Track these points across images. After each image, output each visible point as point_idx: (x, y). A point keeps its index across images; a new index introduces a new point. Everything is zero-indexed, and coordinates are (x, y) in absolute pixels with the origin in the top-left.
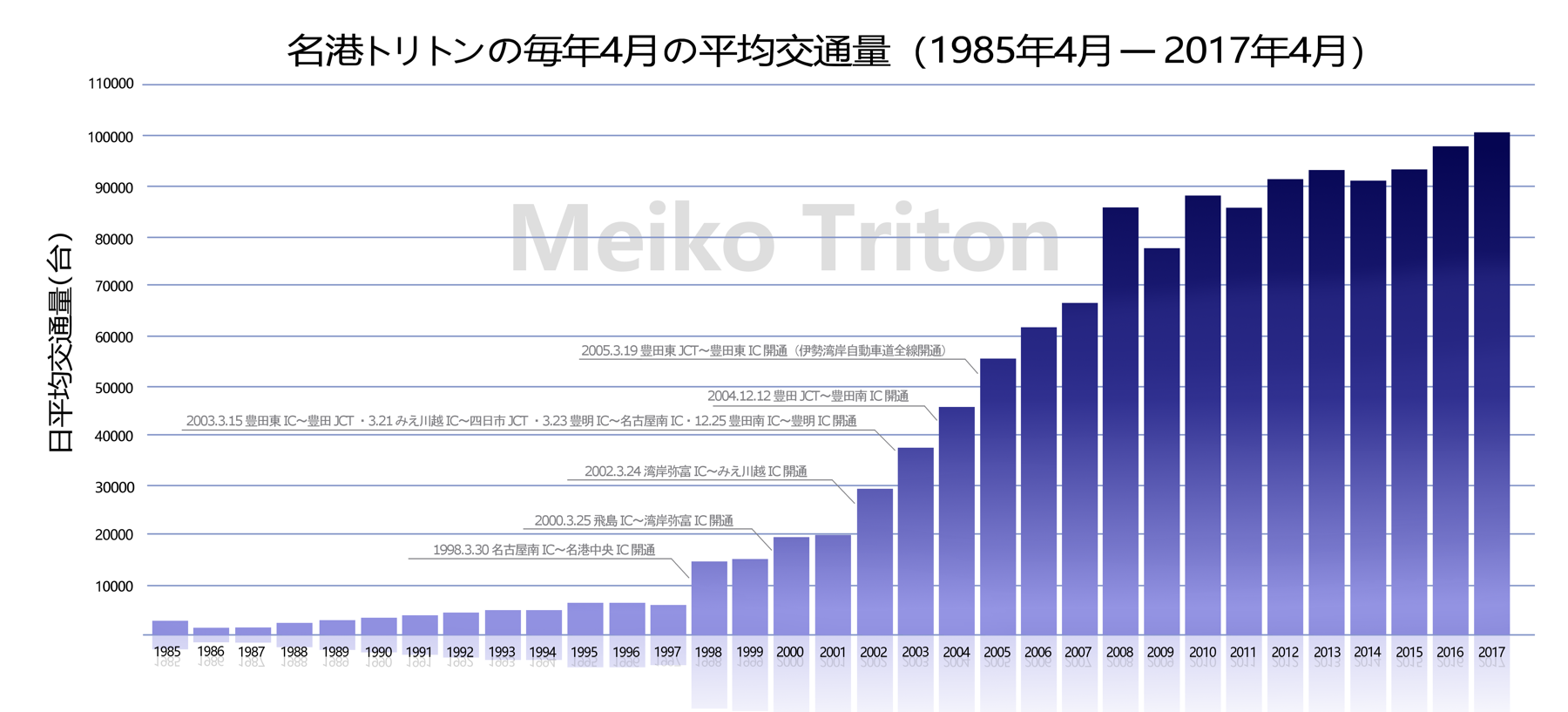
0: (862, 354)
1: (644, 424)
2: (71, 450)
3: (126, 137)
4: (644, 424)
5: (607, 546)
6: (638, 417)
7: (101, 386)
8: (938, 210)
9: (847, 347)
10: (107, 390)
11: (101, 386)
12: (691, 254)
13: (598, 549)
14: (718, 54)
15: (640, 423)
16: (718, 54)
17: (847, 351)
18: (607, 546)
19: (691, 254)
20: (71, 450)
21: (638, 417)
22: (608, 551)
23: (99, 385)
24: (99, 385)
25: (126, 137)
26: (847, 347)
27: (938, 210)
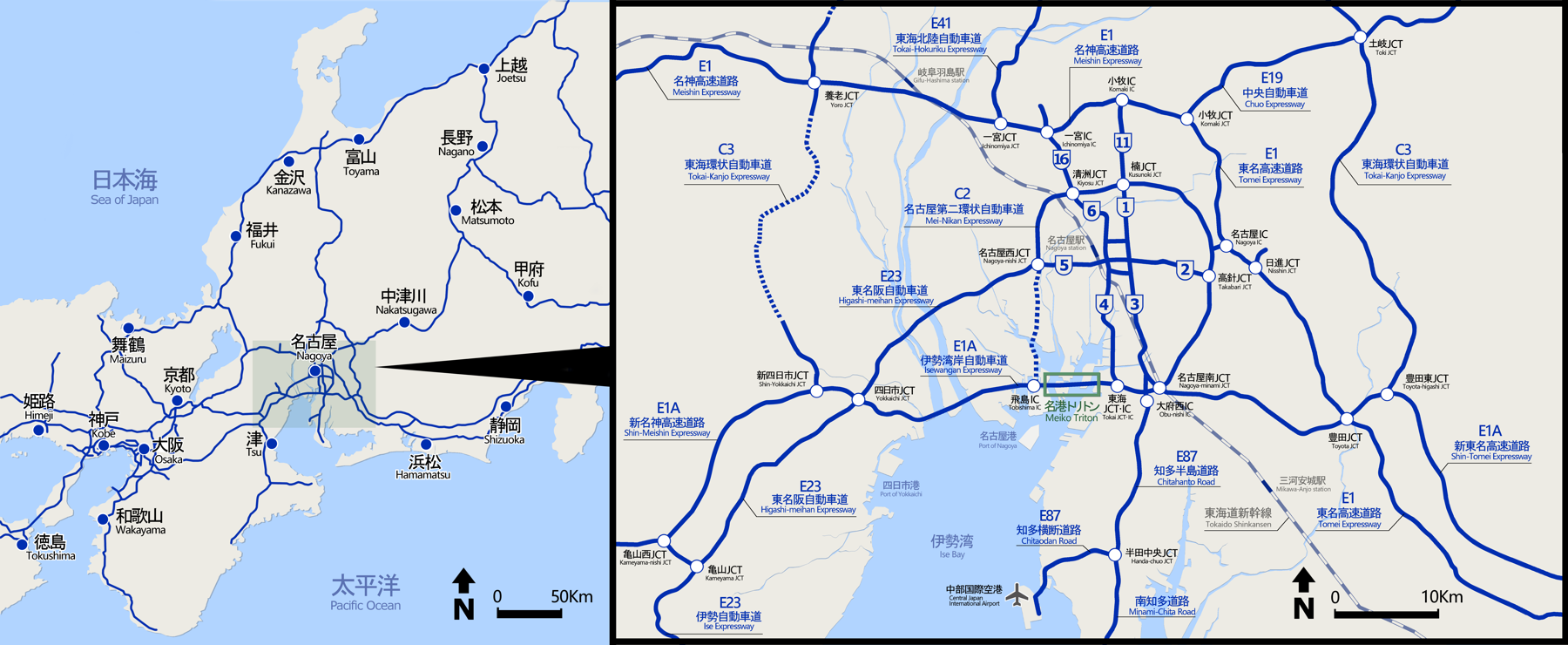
0: (978, 363)
1: (925, 211)
2: (95, 188)
3: (1264, 482)
4: (925, 211)
5: (1259, 90)
6: (920, 206)
7: (558, 594)
8: (464, 571)
9: (964, 357)
10: (564, 599)
11: (558, 594)
12: (1308, 607)
13: (1250, 92)
14: (366, 587)
15: (922, 211)
16: (366, 587)
17: (964, 361)
18: (1259, 90)
19: (1308, 607)
20: (95, 188)
21: (920, 206)
22: (1259, 94)
23: (555, 593)
24: (555, 593)
25: (1264, 482)
26: (964, 357)
27: (464, 571)
